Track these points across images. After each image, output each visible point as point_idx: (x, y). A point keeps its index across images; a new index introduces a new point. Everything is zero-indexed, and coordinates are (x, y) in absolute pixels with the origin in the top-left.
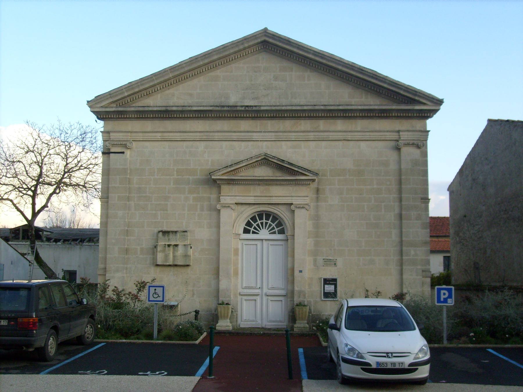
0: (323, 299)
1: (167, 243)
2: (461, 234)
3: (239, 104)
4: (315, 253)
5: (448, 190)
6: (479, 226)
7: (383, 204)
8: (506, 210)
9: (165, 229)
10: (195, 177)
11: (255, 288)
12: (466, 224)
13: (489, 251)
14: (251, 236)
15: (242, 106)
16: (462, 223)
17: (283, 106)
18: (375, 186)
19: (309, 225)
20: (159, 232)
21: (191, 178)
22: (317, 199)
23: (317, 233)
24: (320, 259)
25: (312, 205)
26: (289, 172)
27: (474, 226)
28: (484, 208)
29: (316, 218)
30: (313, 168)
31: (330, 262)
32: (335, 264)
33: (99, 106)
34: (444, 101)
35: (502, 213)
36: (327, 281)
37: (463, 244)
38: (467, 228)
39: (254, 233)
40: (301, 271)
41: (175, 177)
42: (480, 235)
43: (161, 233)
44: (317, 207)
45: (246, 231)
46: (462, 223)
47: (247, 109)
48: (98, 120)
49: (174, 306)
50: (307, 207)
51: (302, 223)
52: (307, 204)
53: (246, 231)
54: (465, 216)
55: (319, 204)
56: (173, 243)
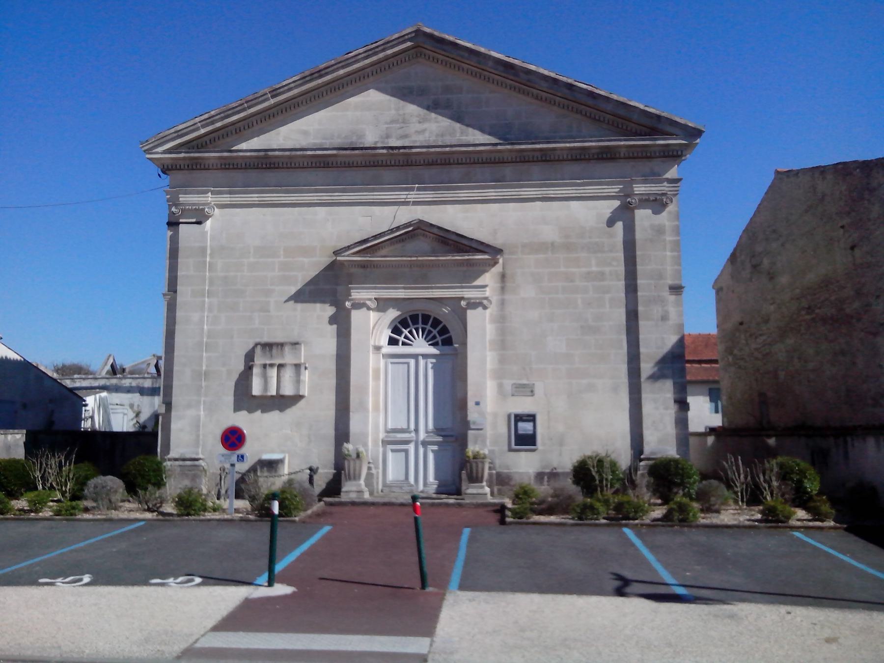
0: (513, 446)
1: (268, 362)
2: (736, 352)
3: (379, 145)
4: (499, 375)
5: (713, 287)
6: (764, 337)
7: (608, 296)
8: (809, 308)
9: (265, 339)
10: (314, 259)
11: (402, 431)
12: (743, 336)
13: (782, 375)
14: (399, 349)
15: (383, 148)
16: (737, 334)
17: (447, 146)
18: (594, 269)
19: (490, 330)
20: (256, 345)
21: (306, 260)
22: (503, 289)
23: (502, 343)
24: (508, 384)
25: (495, 299)
26: (463, 252)
27: (756, 338)
28: (772, 308)
29: (501, 320)
30: (496, 242)
31: (526, 390)
32: (532, 391)
33: (160, 149)
34: (704, 135)
35: (803, 312)
36: (519, 418)
37: (740, 367)
38: (744, 342)
39: (404, 344)
40: (477, 404)
41: (282, 259)
42: (768, 351)
43: (259, 347)
44: (502, 303)
45: (392, 342)
46: (737, 334)
47: (391, 151)
48: (161, 174)
49: (449, 494)
50: (485, 302)
51: (480, 329)
52: (486, 298)
53: (392, 342)
54: (741, 324)
55: (507, 297)
56: (278, 362)
